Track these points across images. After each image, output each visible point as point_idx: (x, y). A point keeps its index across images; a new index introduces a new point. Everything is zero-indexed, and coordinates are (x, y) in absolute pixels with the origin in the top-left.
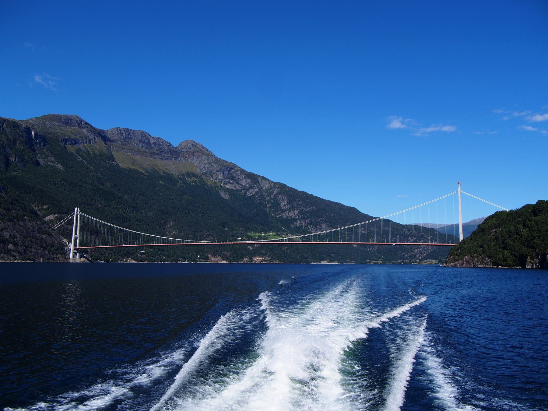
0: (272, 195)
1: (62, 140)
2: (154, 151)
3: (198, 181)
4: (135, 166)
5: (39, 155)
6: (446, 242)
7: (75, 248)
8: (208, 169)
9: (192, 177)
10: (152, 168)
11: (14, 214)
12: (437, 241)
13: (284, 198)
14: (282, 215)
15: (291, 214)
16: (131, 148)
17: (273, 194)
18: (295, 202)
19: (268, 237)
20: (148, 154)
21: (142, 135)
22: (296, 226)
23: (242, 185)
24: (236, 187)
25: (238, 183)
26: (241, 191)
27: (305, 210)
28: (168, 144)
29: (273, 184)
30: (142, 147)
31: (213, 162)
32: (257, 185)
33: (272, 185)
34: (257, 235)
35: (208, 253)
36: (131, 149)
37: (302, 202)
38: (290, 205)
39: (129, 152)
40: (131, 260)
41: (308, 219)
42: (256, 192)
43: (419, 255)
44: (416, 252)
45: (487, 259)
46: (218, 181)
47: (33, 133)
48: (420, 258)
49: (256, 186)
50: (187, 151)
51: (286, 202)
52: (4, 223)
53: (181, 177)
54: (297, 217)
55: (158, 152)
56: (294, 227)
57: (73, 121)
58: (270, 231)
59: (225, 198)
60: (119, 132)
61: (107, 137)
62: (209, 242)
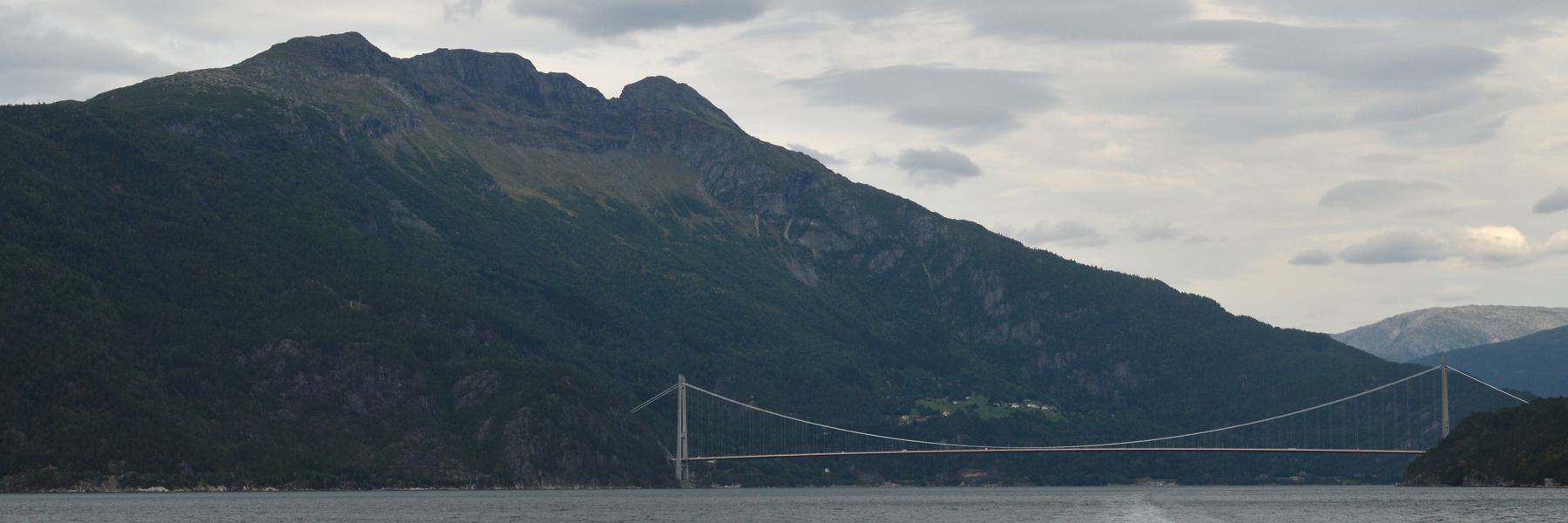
8: (736, 183)
23: (850, 237)
24: (831, 244)
28: (595, 97)
37: (1048, 293)
49: (896, 238)
51: (999, 293)
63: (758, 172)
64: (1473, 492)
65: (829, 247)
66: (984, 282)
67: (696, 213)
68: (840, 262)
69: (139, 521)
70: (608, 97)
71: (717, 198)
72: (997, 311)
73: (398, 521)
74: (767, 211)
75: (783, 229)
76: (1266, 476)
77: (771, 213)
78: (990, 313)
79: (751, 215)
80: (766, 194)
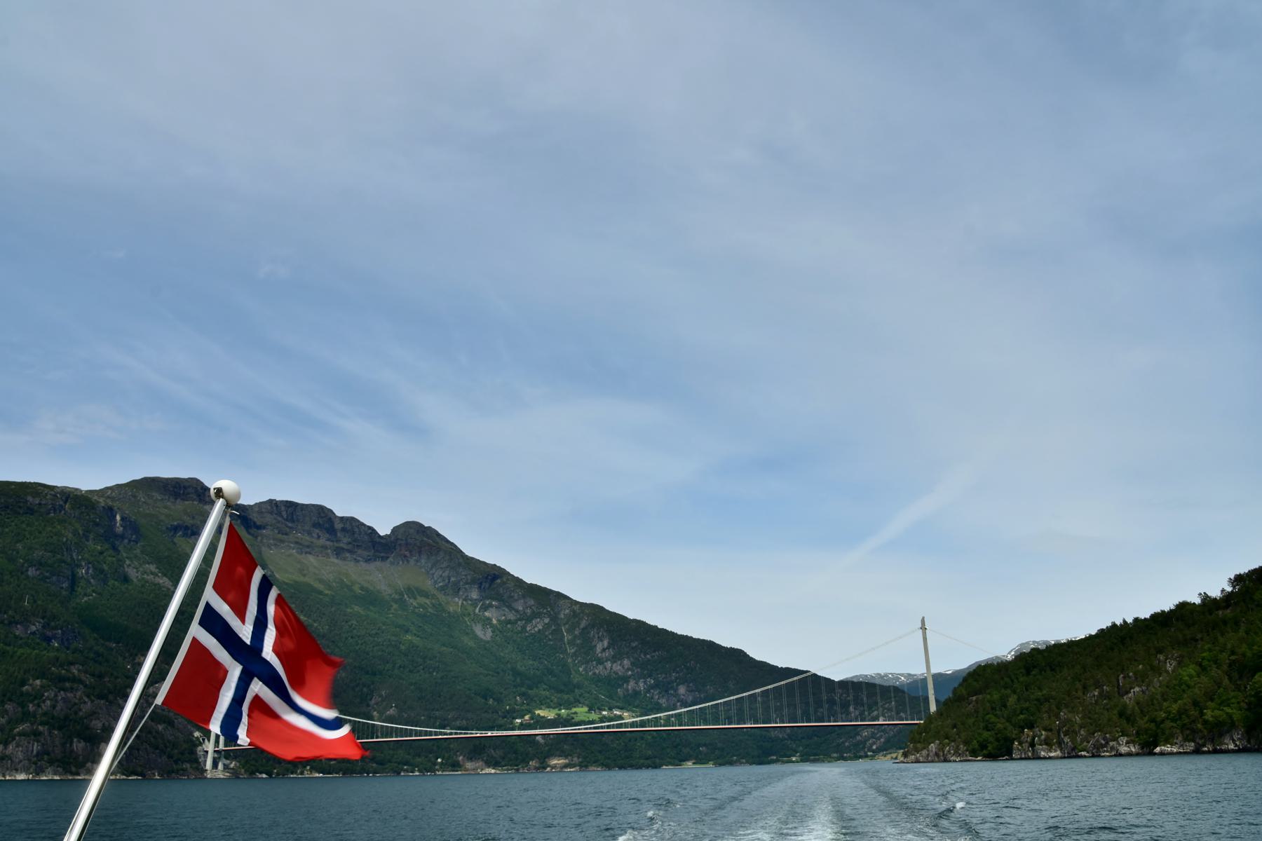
0: (577, 629)
1: (167, 528)
2: (341, 545)
3: (429, 603)
4: (304, 575)
5: (128, 562)
6: (826, 718)
7: (216, 749)
8: (449, 580)
9: (418, 597)
10: (337, 580)
11: (109, 685)
12: (905, 712)
13: (603, 635)
14: (599, 670)
15: (617, 667)
16: (297, 540)
17: (579, 627)
18: (624, 642)
19: (573, 715)
20: (329, 551)
21: (319, 514)
22: (628, 690)
23: (517, 611)
24: (504, 615)
25: (511, 608)
26: (515, 622)
27: (642, 659)
28: (370, 531)
29: (578, 606)
30: (319, 537)
31: (460, 564)
32: (547, 609)
33: (576, 608)
34: (549, 714)
35: (458, 753)
36: (297, 543)
37: (636, 643)
38: (614, 649)
39: (293, 549)
40: (311, 772)
41: (650, 676)
42: (546, 624)
43: (871, 741)
44: (865, 736)
45: (962, 746)
46: (470, 602)
47: (118, 518)
48: (874, 747)
49: (545, 611)
50: (407, 544)
51: (606, 643)
52: (92, 701)
53: (397, 597)
54: (630, 673)
55: (350, 547)
56: (624, 694)
57: (190, 490)
58: (577, 702)
59: (484, 638)
60: (275, 508)
61: (251, 520)
62: (465, 734)
63: (463, 573)
64: (960, 767)
65: (503, 618)
66: (597, 636)
67: (421, 596)
68: (509, 626)
70: (382, 533)
71: (438, 589)
72: (604, 654)
75: (476, 607)
76: (775, 758)
78: (600, 655)
79: (457, 599)
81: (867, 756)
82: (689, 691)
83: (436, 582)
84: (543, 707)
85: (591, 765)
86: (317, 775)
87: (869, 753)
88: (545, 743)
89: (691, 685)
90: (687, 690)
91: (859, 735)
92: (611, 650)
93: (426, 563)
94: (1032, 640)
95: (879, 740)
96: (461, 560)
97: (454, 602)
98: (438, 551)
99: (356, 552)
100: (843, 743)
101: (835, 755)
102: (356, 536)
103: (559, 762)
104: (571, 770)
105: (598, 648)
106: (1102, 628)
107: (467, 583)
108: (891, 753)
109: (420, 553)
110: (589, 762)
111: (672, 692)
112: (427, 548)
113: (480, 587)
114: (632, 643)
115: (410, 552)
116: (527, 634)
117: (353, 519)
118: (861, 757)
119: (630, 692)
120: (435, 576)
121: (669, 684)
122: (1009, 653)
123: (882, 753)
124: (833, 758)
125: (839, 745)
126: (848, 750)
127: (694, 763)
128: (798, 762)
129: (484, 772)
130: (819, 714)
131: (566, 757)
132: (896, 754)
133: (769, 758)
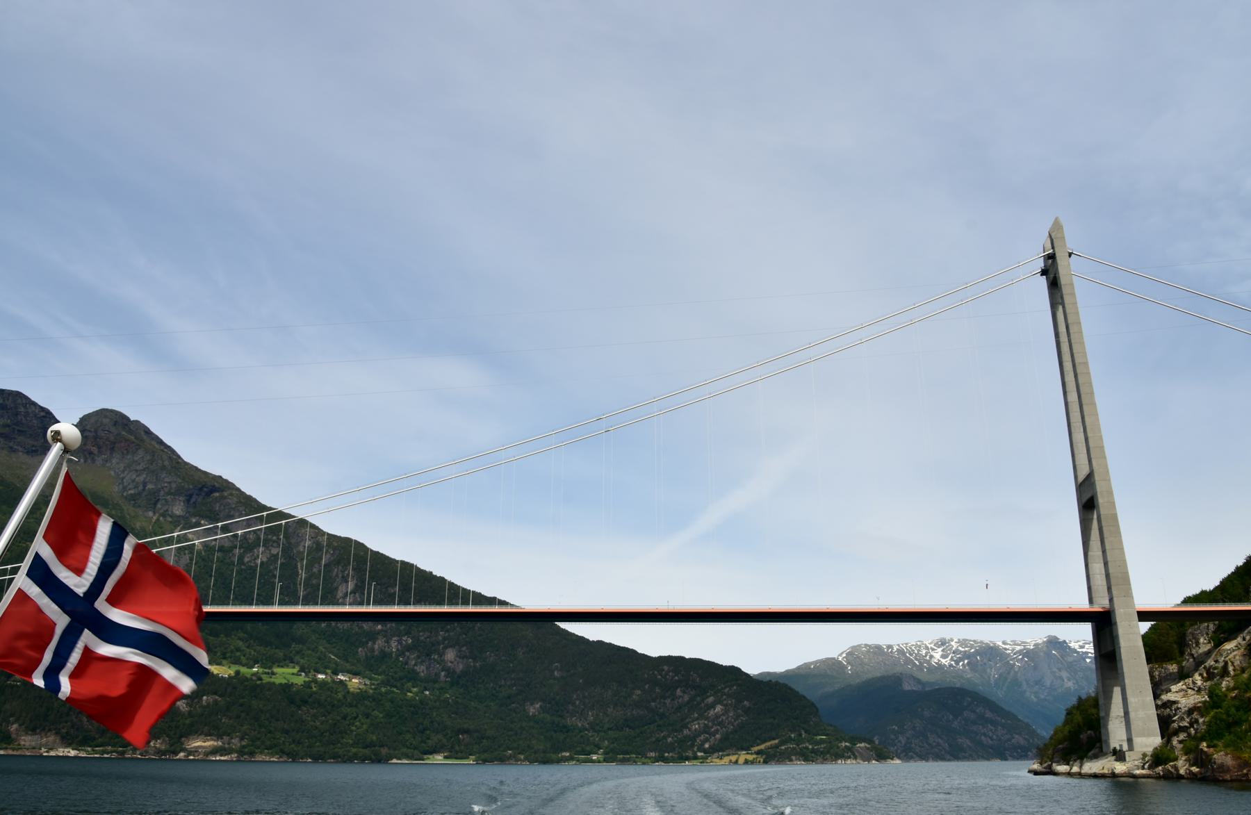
8: (145, 487)
22: (373, 650)
28: (42, 414)
31: (163, 468)
43: (702, 737)
44: (696, 730)
46: (170, 519)
48: (707, 746)
63: (166, 480)
66: (340, 576)
69: (684, 813)
73: (229, 813)
74: (167, 510)
76: (568, 754)
77: (170, 513)
80: (169, 497)
81: (696, 758)
82: (460, 658)
83: (125, 489)
84: (224, 662)
85: (261, 753)
86: (62, 752)
87: (699, 754)
88: (190, 712)
89: (464, 649)
90: (457, 656)
91: (687, 728)
92: (357, 595)
93: (118, 463)
94: (864, 643)
95: (714, 736)
96: (166, 463)
97: (146, 517)
98: (137, 449)
99: (15, 438)
100: (665, 738)
101: (653, 754)
102: (19, 417)
103: (203, 744)
104: (222, 758)
105: (339, 592)
106: (945, 636)
107: (169, 493)
108: (728, 755)
109: (112, 449)
110: (258, 748)
111: (436, 657)
112: (123, 444)
113: (188, 501)
114: (389, 589)
115: (99, 448)
116: (243, 567)
117: (18, 395)
118: (688, 759)
119: (376, 653)
120: (125, 480)
121: (433, 645)
122: (841, 655)
123: (716, 755)
124: (650, 758)
125: (658, 740)
126: (671, 748)
127: (446, 757)
128: (599, 762)
129: (52, 753)
130: (634, 697)
131: (219, 737)
132: (737, 756)
133: (560, 755)
